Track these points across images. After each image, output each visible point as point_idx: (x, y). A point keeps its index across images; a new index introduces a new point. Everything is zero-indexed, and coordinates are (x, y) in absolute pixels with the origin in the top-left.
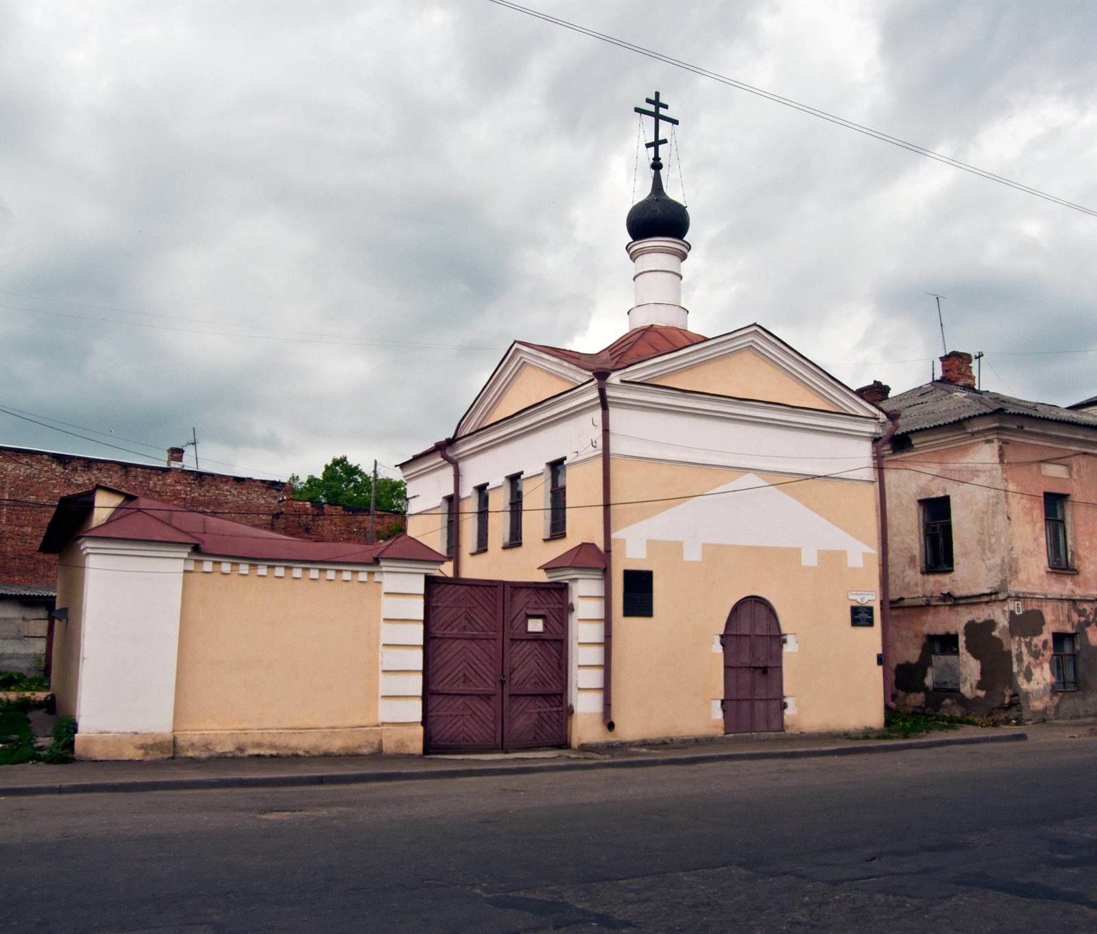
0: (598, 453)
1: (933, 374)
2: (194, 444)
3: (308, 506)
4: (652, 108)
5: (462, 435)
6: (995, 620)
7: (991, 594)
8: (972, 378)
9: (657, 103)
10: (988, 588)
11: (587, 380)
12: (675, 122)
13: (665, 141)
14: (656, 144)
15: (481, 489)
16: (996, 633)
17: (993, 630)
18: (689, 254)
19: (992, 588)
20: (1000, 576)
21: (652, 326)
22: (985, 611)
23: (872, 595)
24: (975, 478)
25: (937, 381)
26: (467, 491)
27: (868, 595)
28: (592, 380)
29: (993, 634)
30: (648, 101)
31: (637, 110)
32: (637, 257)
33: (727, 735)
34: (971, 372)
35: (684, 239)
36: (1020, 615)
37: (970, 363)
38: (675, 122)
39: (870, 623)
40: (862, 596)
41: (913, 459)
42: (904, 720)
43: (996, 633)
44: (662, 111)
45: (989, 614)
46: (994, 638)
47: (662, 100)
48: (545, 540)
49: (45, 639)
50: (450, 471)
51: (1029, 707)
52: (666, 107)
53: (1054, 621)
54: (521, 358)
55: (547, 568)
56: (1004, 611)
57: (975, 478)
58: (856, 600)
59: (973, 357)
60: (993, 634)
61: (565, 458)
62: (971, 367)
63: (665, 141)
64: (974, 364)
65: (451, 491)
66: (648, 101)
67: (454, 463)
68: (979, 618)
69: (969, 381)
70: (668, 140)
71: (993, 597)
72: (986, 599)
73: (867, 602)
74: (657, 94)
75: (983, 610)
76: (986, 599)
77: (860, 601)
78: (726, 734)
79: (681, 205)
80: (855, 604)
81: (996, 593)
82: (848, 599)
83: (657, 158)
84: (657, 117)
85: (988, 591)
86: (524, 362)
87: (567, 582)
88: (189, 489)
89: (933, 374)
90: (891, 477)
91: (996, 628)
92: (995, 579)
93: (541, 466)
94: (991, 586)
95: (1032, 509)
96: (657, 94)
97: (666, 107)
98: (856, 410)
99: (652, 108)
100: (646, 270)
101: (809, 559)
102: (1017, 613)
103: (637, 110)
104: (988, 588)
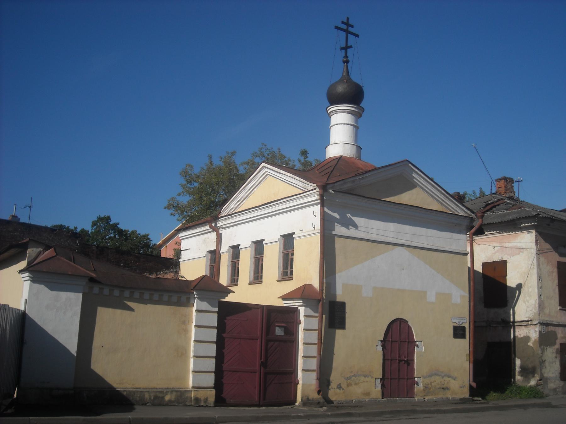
0: (317, 231)
1: (491, 189)
2: (30, 207)
3: (94, 248)
4: (344, 27)
5: (223, 215)
6: (530, 336)
7: (528, 321)
8: (514, 193)
9: (347, 24)
10: (526, 317)
11: (312, 189)
12: (357, 36)
13: (351, 47)
14: (346, 48)
15: (235, 249)
16: (530, 344)
17: (529, 342)
18: (363, 114)
19: (528, 317)
20: (534, 311)
21: (341, 156)
22: (524, 330)
23: (465, 319)
24: (521, 253)
25: (493, 194)
26: (225, 248)
27: (463, 319)
28: (316, 189)
29: (529, 344)
30: (343, 23)
31: (337, 28)
32: (332, 116)
33: (383, 399)
34: (513, 189)
35: (360, 105)
36: (544, 333)
37: (513, 184)
38: (357, 36)
39: (463, 336)
40: (460, 320)
41: (483, 240)
42: (559, 391)
43: (530, 344)
44: (350, 29)
45: (527, 332)
46: (529, 346)
47: (351, 22)
48: (278, 281)
49: (316, 346)
50: (214, 235)
51: (548, 387)
52: (352, 26)
53: (562, 338)
54: (266, 171)
55: (284, 298)
56: (536, 331)
57: (521, 253)
58: (456, 322)
59: (515, 181)
60: (529, 344)
61: (294, 233)
62: (513, 186)
63: (351, 47)
64: (515, 185)
65: (214, 248)
66: (343, 23)
67: (216, 229)
68: (521, 335)
69: (512, 195)
70: (353, 46)
71: (529, 322)
72: (525, 323)
73: (462, 324)
74: (348, 19)
75: (523, 330)
76: (525, 323)
77: (458, 323)
78: (383, 398)
79: (360, 86)
80: (455, 325)
81: (531, 321)
82: (452, 321)
83: (346, 56)
84: (347, 32)
85: (526, 319)
86: (268, 174)
87: (297, 306)
88: (22, 235)
89: (491, 189)
90: (359, 230)
91: (530, 341)
92: (531, 312)
93: (276, 236)
94: (528, 316)
95: (553, 272)
96: (348, 19)
97: (352, 26)
98: (459, 212)
99: (344, 27)
100: (338, 123)
101: (431, 297)
102: (543, 332)
103: (337, 28)
104: (526, 317)
